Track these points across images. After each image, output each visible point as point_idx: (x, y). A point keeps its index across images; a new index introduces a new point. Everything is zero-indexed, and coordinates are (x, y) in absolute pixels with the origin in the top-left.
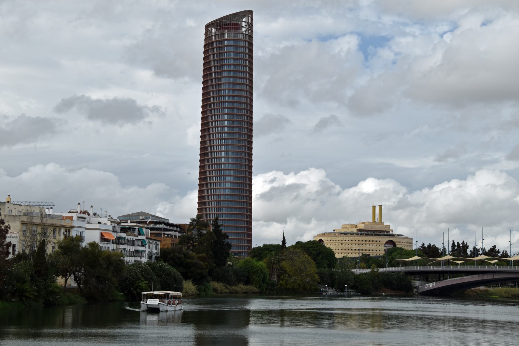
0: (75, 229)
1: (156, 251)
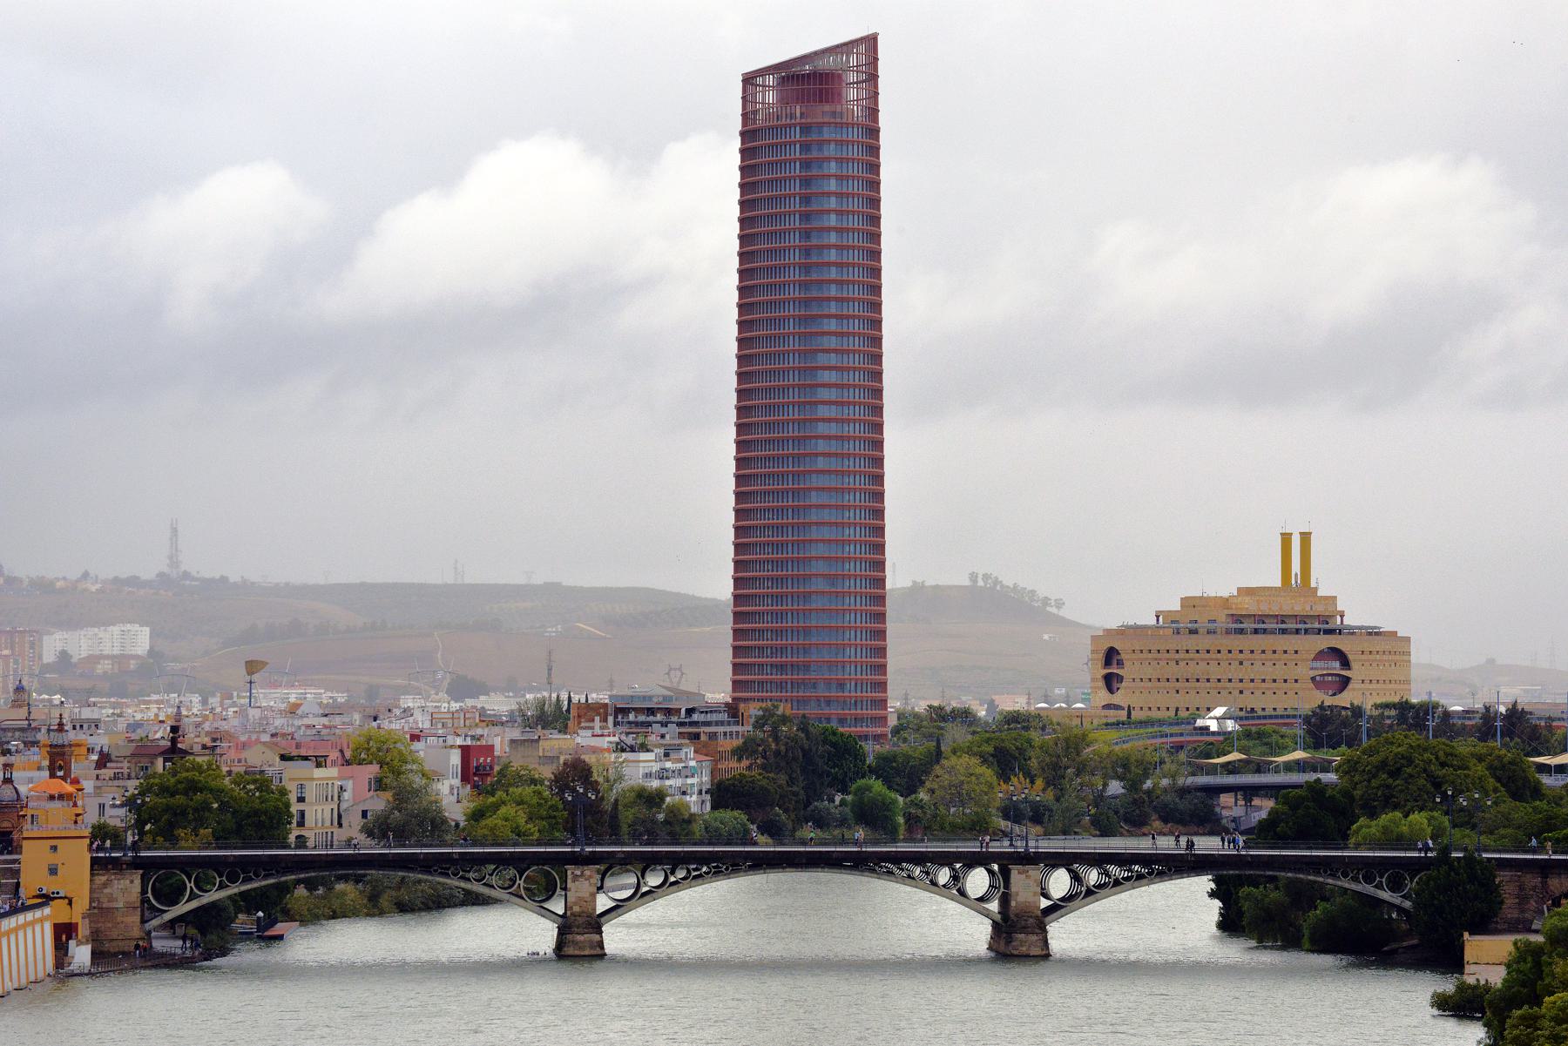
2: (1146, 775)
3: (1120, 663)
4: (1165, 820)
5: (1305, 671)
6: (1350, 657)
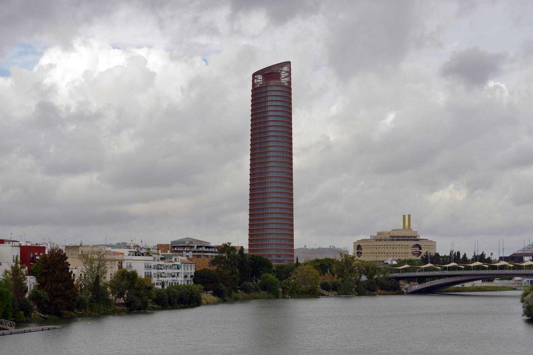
0: (126, 261)
1: (192, 271)
2: (375, 273)
3: (361, 249)
4: (382, 289)
5: (410, 251)
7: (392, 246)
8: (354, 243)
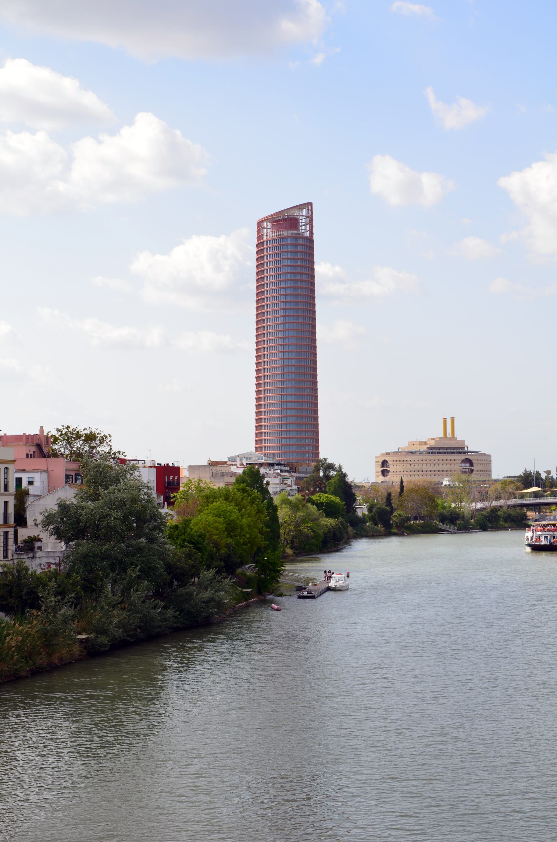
3: (387, 466)
6: (474, 462)
7: (432, 461)
8: (377, 457)
